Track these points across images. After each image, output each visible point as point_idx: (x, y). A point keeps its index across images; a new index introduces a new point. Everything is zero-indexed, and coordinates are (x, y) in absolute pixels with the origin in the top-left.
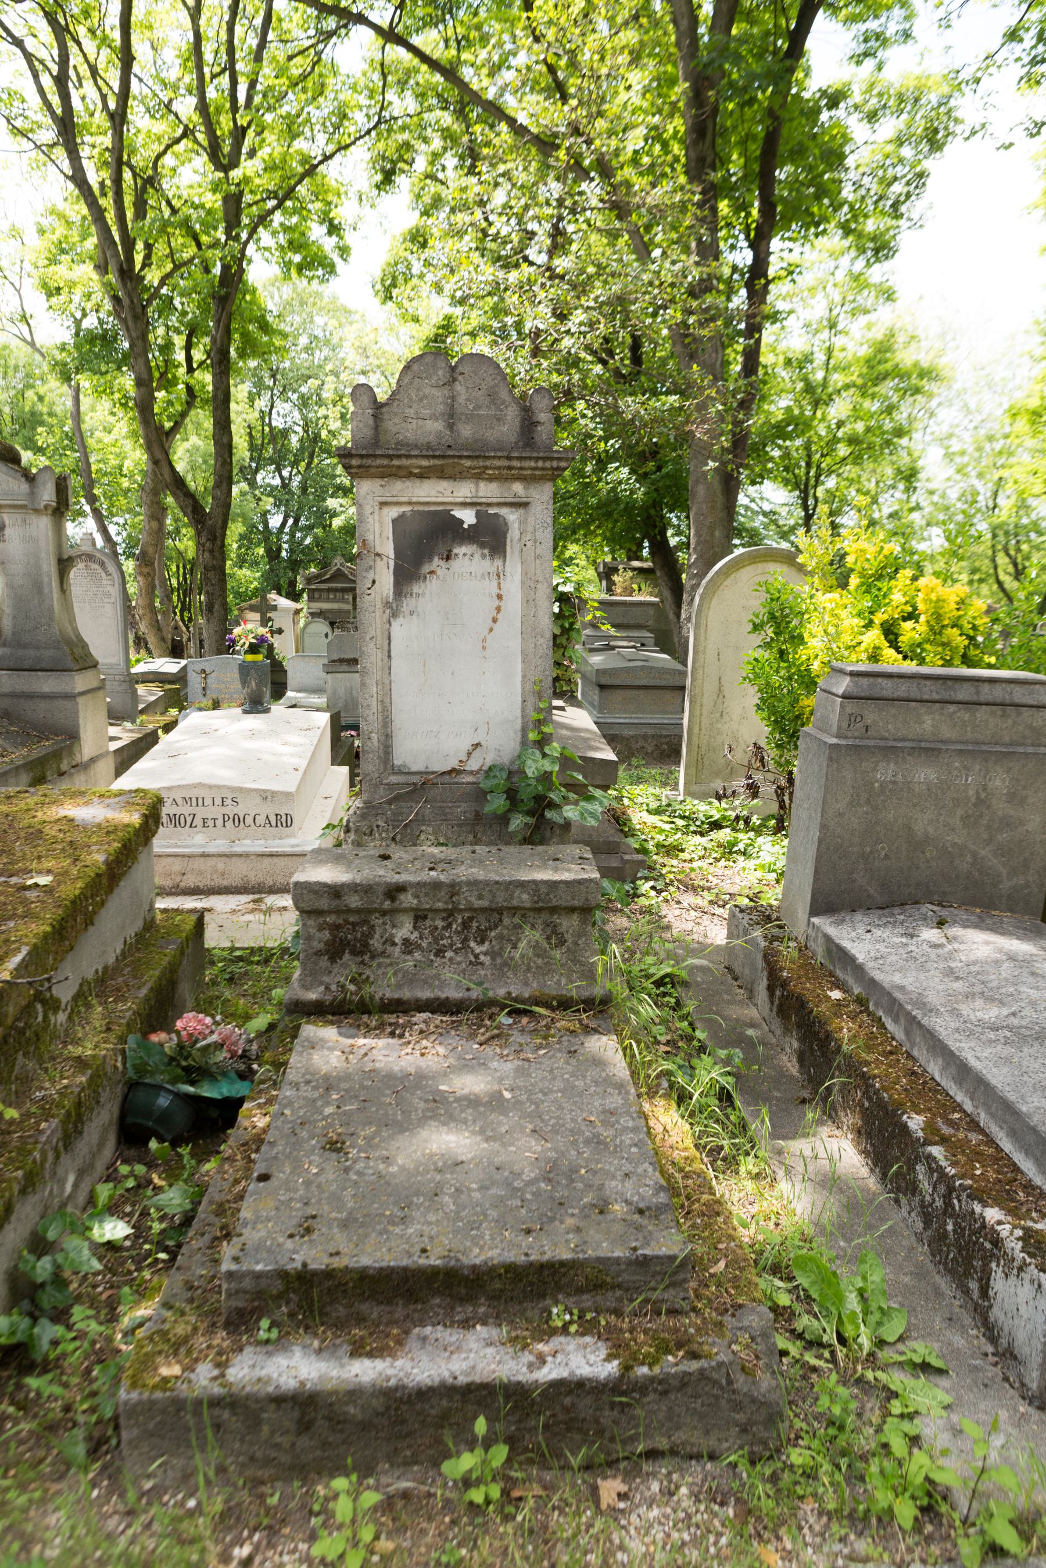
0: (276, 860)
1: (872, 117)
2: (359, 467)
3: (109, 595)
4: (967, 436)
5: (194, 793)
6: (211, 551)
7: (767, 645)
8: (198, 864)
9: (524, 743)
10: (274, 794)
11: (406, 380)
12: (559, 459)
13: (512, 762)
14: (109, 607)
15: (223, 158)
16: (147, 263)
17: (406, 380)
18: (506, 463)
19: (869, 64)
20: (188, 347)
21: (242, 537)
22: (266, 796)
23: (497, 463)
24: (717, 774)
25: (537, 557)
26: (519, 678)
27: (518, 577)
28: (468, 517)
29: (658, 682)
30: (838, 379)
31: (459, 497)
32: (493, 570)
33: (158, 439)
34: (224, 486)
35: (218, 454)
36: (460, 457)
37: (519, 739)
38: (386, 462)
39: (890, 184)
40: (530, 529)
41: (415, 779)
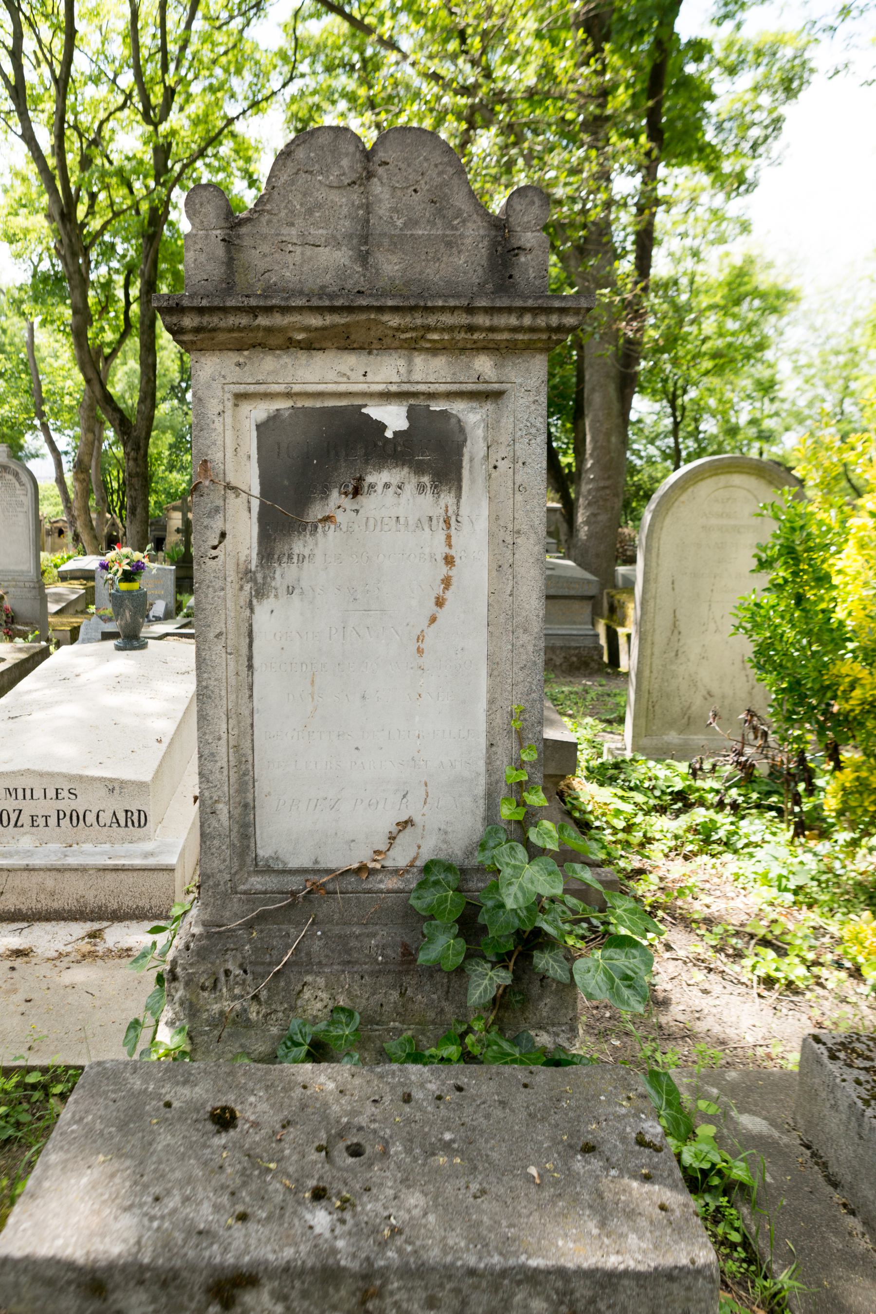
0: (122, 875)
1: (732, 71)
2: (198, 330)
3: (22, 504)
4: (815, 352)
5: (20, 783)
6: (135, 460)
7: (778, 588)
8: (19, 881)
9: (491, 817)
10: (123, 783)
11: (284, 178)
12: (563, 311)
13: (468, 853)
14: (21, 515)
15: (152, 116)
16: (91, 212)
17: (284, 178)
18: (463, 319)
19: (729, 25)
20: (127, 286)
21: (171, 446)
22: (113, 787)
23: (448, 319)
24: (671, 724)
25: (519, 488)
26: (483, 705)
27: (482, 525)
28: (393, 418)
29: (566, 592)
30: (704, 301)
31: (378, 383)
32: (438, 512)
33: (93, 362)
34: (148, 402)
35: (144, 373)
36: (381, 309)
37: (481, 811)
38: (244, 320)
39: (749, 128)
40: (505, 438)
41: (294, 883)
